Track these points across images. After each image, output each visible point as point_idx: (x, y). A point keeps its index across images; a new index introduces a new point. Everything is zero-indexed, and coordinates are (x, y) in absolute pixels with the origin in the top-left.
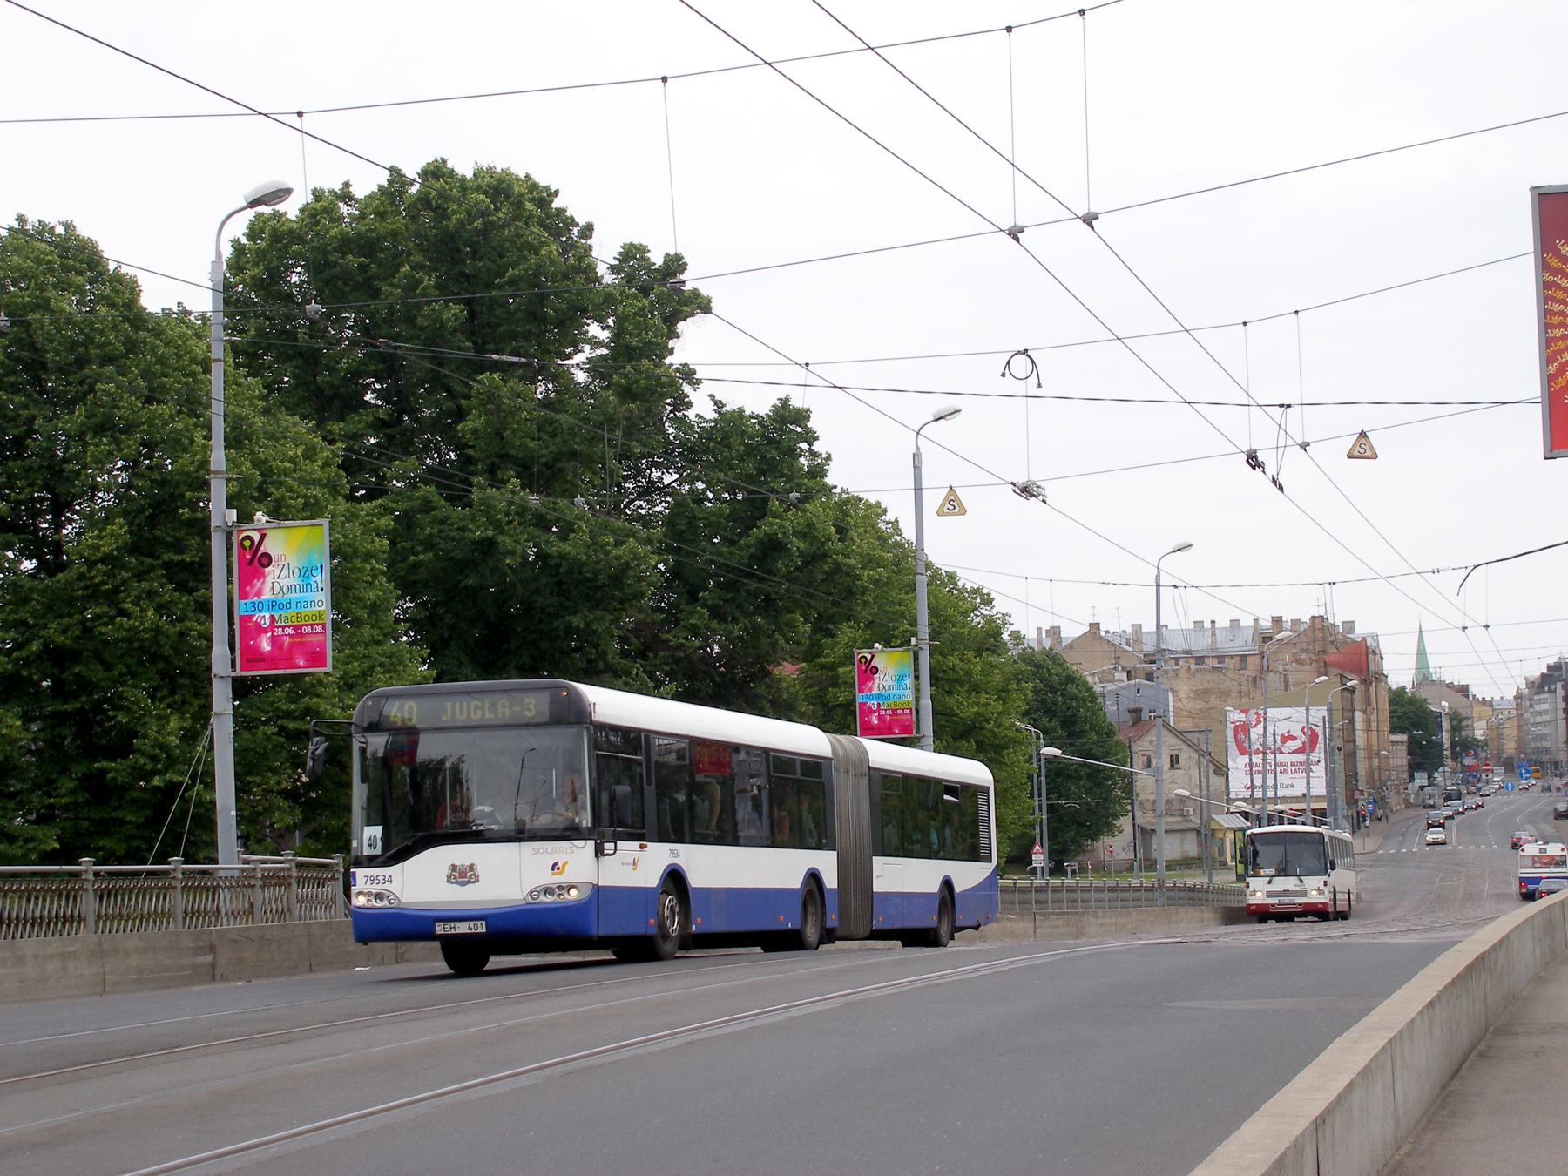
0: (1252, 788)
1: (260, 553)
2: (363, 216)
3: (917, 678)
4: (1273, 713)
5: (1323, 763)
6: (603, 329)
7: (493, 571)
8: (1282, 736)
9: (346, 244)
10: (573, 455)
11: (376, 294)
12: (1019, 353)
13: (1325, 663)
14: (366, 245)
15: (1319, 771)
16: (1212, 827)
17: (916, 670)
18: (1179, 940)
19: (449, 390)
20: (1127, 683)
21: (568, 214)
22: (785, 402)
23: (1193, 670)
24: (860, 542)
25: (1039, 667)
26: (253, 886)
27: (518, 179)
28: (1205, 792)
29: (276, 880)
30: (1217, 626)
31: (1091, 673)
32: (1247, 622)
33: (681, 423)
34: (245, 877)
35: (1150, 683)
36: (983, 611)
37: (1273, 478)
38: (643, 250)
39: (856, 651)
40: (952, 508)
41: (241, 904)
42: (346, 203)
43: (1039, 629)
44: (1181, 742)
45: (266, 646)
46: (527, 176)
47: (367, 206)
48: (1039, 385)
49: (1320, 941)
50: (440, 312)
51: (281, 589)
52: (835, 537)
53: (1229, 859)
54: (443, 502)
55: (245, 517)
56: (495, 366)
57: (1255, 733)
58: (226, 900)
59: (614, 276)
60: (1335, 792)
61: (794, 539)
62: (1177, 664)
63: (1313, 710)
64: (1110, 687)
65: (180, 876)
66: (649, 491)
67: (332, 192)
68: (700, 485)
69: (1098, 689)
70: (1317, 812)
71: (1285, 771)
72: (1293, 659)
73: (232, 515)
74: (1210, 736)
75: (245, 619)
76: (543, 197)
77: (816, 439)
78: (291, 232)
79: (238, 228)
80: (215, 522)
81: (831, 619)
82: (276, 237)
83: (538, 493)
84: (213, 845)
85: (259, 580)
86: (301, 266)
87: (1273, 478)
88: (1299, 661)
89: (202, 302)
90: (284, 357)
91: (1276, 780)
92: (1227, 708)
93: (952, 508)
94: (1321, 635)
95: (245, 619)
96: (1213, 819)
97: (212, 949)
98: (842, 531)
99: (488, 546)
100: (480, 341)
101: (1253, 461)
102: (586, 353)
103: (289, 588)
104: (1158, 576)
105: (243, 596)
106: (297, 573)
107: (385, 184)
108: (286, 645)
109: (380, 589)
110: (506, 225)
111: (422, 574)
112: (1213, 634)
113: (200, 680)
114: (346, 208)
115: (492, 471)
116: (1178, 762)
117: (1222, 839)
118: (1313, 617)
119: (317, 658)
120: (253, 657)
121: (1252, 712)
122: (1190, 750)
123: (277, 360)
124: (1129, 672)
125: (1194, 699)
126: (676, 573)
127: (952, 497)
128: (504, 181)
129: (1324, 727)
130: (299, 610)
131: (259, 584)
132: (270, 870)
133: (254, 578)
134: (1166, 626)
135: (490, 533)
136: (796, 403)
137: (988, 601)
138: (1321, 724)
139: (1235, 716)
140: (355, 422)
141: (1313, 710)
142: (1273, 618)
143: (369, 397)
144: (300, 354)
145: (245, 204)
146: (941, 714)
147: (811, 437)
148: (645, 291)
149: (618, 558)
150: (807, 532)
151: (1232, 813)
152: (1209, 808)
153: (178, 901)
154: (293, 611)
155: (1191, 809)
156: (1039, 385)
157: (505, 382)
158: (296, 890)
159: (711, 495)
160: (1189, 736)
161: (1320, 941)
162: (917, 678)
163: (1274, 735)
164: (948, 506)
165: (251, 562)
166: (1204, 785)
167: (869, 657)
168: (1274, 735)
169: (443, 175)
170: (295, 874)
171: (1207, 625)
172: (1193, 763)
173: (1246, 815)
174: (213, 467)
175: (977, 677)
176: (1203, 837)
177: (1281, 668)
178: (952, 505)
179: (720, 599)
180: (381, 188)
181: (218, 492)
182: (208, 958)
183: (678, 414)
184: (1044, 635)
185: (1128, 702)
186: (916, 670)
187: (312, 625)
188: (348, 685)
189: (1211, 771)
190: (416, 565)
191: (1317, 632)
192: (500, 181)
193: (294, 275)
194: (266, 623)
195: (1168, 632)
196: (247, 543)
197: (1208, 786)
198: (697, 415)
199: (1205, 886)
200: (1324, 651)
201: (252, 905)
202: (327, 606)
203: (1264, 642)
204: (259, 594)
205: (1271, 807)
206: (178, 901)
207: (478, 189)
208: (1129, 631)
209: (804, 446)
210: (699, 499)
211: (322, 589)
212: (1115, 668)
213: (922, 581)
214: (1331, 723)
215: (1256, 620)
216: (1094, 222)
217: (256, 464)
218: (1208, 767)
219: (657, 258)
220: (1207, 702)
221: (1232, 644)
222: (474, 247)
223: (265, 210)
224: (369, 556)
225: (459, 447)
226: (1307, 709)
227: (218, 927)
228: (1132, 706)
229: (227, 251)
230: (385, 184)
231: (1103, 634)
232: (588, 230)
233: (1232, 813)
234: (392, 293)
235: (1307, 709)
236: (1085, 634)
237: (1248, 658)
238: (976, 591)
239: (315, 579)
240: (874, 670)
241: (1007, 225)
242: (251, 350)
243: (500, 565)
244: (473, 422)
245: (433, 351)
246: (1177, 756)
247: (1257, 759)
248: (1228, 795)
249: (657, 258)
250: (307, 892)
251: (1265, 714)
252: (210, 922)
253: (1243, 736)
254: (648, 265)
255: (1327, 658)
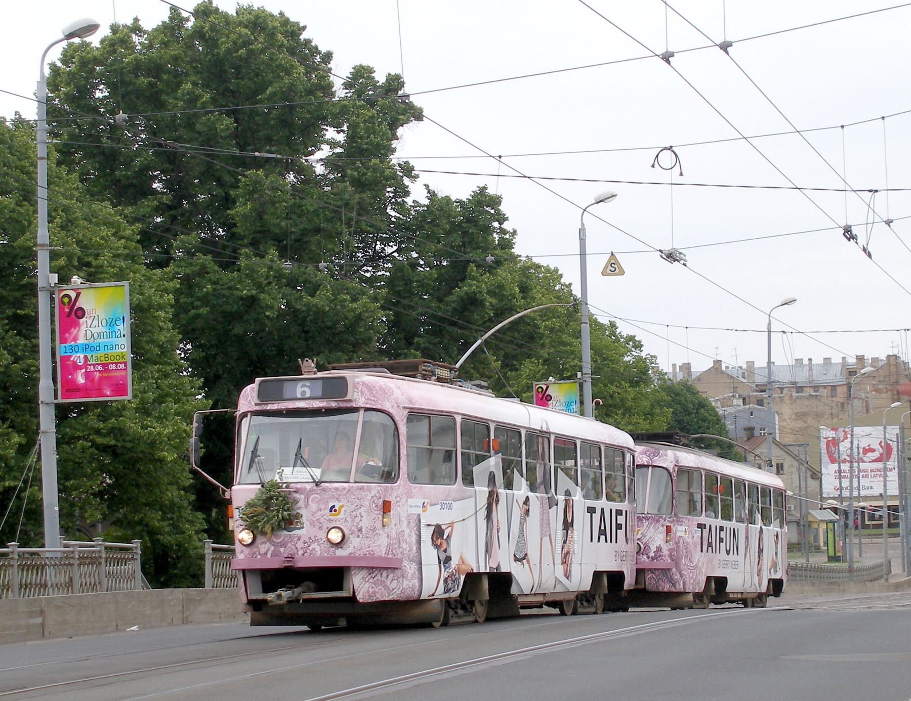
0: (841, 489)
1: (76, 308)
2: (150, 46)
3: (582, 403)
4: (858, 430)
5: (896, 469)
6: (338, 132)
7: (256, 320)
8: (864, 448)
9: (137, 67)
10: (318, 230)
11: (160, 105)
12: (665, 148)
13: (898, 391)
14: (155, 69)
15: (893, 476)
16: (809, 520)
17: (581, 395)
18: (788, 607)
19: (219, 181)
20: (742, 407)
21: (313, 44)
22: (483, 189)
23: (794, 398)
24: (583, 306)
25: (677, 394)
26: (72, 565)
27: (272, 16)
28: (803, 492)
29: (84, 560)
30: (813, 362)
31: (715, 398)
32: (837, 359)
33: (401, 207)
34: (67, 558)
35: (761, 407)
36: (634, 353)
37: (864, 248)
38: (370, 71)
39: (535, 383)
40: (613, 269)
41: (63, 579)
42: (137, 34)
43: (674, 365)
44: (784, 454)
45: (81, 380)
46: (281, 14)
47: (155, 38)
48: (681, 174)
49: (898, 609)
50: (214, 123)
51: (93, 335)
52: (519, 295)
53: (822, 544)
54: (216, 268)
55: (64, 280)
56: (258, 163)
57: (844, 446)
58: (51, 576)
59: (347, 91)
60: (906, 493)
61: (488, 297)
62: (782, 393)
63: (889, 428)
64: (730, 410)
65: (17, 557)
66: (375, 259)
67: (125, 26)
68: (415, 255)
69: (720, 411)
70: (891, 508)
71: (867, 476)
72: (872, 389)
73: (54, 278)
74: (808, 449)
75: (65, 359)
76: (293, 31)
77: (507, 219)
78: (95, 59)
79: (55, 56)
80: (41, 283)
81: (514, 357)
82: (84, 63)
83: (292, 259)
84: (41, 535)
85: (75, 329)
86: (103, 84)
87: (864, 248)
88: (877, 390)
89: (31, 112)
90: (89, 155)
91: (859, 483)
92: (821, 427)
93: (613, 269)
94: (894, 370)
95: (65, 359)
96: (809, 513)
97: (42, 612)
98: (524, 289)
99: (252, 302)
100: (242, 143)
101: (849, 235)
102: (325, 152)
103: (99, 334)
104: (769, 324)
105: (63, 340)
106: (104, 322)
107: (167, 20)
108: (96, 378)
109: (167, 333)
110: (263, 51)
111: (199, 324)
112: (810, 369)
113: (32, 403)
114: (137, 38)
115: (254, 244)
116: (782, 469)
117: (816, 529)
118: (889, 356)
119: (120, 389)
120: (70, 388)
121: (841, 430)
122: (792, 459)
123: (84, 157)
124: (744, 399)
125: (795, 420)
126: (395, 324)
127: (613, 261)
128: (260, 17)
129: (898, 442)
130: (106, 352)
131: (75, 331)
132: (85, 552)
133: (71, 327)
134: (774, 363)
135: (254, 292)
136: (491, 191)
137: (638, 346)
138: (895, 440)
139: (827, 433)
140: (147, 205)
141: (889, 428)
142: (857, 356)
143: (156, 185)
144: (103, 153)
145: (63, 37)
146: (366, 421)
147: (502, 219)
148: (371, 103)
149: (354, 310)
150: (498, 291)
151: (825, 509)
152: (807, 506)
153: (15, 576)
154: (101, 353)
155: (793, 506)
156: (681, 174)
157: (267, 176)
158: (105, 569)
159: (422, 263)
160: (791, 448)
161: (898, 609)
162: (582, 403)
163: (858, 448)
164: (610, 268)
165: (69, 315)
166: (803, 486)
167: (544, 387)
168: (858, 448)
169: (211, 13)
170: (104, 556)
171: (806, 362)
172: (794, 470)
173: (835, 510)
174: (39, 241)
175: (629, 403)
176: (802, 527)
177: (863, 396)
178: (613, 267)
179: (430, 343)
180: (164, 23)
181: (43, 260)
182: (39, 620)
183: (399, 200)
184: (678, 370)
185: (743, 423)
186: (581, 395)
187: (116, 364)
188: (144, 410)
189: (809, 476)
190: (197, 316)
191: (892, 368)
192: (257, 17)
193: (98, 91)
194: (81, 362)
195: (775, 368)
196: (66, 300)
197: (806, 487)
198: (414, 201)
199: (805, 565)
200: (897, 382)
201: (71, 579)
202: (127, 348)
203: (850, 375)
204: (75, 339)
205: (856, 504)
206: (15, 576)
207: (241, 24)
208: (744, 366)
209: (496, 224)
210: (414, 265)
211: (124, 336)
212: (733, 396)
213: (585, 329)
214: (903, 438)
215: (844, 358)
216: (729, 49)
217: (79, 242)
218: (806, 473)
219: (380, 78)
220: (805, 422)
221: (825, 377)
222: (238, 68)
223: (76, 40)
224: (161, 307)
225: (229, 226)
226: (885, 428)
227: (46, 596)
228: (747, 425)
229: (47, 72)
230: (167, 20)
231: (724, 369)
232: (328, 57)
233: (825, 509)
234: (176, 106)
235: (885, 428)
236: (710, 369)
237: (838, 388)
238: (631, 338)
239: (118, 327)
240: (549, 398)
241: (661, 51)
242: (65, 150)
243: (260, 316)
244: (241, 209)
245: (207, 150)
246: (782, 464)
247: (845, 467)
248: (821, 495)
249: (380, 78)
250: (113, 569)
251: (852, 432)
252: (40, 592)
253: (833, 449)
254: (375, 86)
255: (900, 388)
